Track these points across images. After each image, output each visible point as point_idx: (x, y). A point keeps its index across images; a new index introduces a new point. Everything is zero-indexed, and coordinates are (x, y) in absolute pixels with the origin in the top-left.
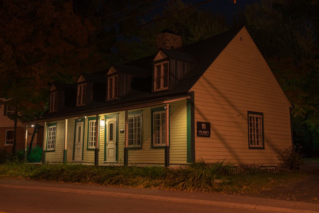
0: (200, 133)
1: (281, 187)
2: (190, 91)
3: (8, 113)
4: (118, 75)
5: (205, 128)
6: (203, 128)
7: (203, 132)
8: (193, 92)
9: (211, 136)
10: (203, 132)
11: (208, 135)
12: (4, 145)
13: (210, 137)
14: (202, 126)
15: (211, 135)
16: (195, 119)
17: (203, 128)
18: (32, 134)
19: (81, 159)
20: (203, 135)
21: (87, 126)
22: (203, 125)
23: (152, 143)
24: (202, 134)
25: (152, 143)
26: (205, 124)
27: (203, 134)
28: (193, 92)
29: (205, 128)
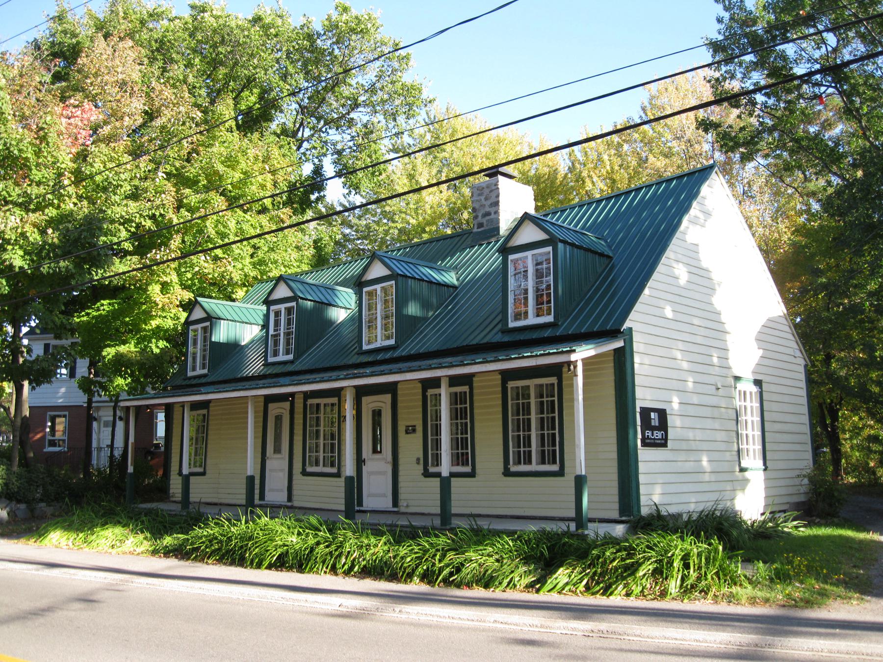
0: (648, 436)
1: (795, 553)
2: (625, 327)
3: (554, 396)
4: (393, 282)
5: (657, 424)
6: (653, 424)
7: (653, 435)
8: (630, 329)
9: (669, 443)
10: (653, 435)
11: (663, 441)
12: (45, 450)
13: (667, 447)
14: (650, 419)
15: (669, 442)
16: (637, 402)
17: (653, 424)
18: (111, 424)
19: (286, 500)
20: (652, 441)
21: (301, 438)
22: (653, 415)
23: (266, 357)
24: (651, 439)
25: (266, 357)
26: (656, 414)
27: (654, 439)
28: (630, 329)
29: (657, 424)
